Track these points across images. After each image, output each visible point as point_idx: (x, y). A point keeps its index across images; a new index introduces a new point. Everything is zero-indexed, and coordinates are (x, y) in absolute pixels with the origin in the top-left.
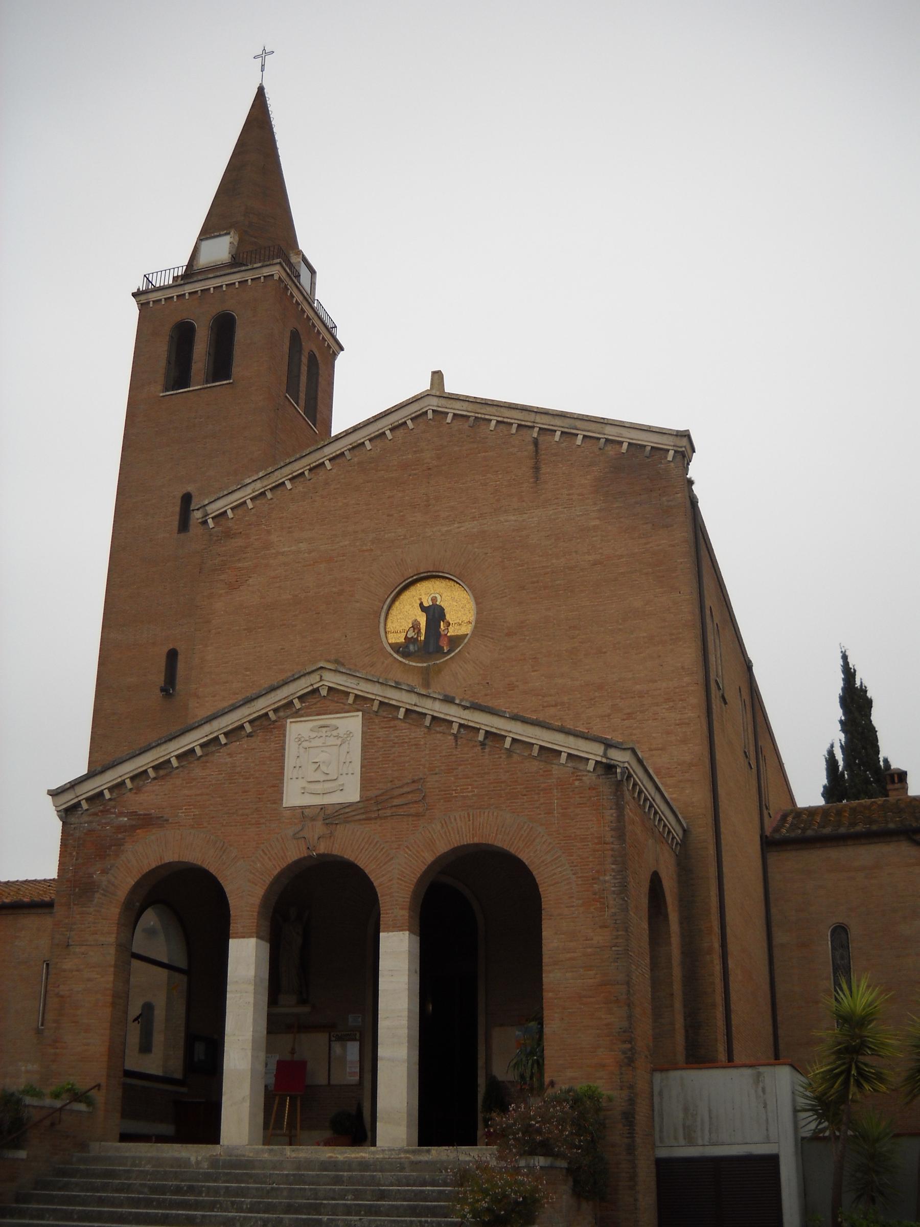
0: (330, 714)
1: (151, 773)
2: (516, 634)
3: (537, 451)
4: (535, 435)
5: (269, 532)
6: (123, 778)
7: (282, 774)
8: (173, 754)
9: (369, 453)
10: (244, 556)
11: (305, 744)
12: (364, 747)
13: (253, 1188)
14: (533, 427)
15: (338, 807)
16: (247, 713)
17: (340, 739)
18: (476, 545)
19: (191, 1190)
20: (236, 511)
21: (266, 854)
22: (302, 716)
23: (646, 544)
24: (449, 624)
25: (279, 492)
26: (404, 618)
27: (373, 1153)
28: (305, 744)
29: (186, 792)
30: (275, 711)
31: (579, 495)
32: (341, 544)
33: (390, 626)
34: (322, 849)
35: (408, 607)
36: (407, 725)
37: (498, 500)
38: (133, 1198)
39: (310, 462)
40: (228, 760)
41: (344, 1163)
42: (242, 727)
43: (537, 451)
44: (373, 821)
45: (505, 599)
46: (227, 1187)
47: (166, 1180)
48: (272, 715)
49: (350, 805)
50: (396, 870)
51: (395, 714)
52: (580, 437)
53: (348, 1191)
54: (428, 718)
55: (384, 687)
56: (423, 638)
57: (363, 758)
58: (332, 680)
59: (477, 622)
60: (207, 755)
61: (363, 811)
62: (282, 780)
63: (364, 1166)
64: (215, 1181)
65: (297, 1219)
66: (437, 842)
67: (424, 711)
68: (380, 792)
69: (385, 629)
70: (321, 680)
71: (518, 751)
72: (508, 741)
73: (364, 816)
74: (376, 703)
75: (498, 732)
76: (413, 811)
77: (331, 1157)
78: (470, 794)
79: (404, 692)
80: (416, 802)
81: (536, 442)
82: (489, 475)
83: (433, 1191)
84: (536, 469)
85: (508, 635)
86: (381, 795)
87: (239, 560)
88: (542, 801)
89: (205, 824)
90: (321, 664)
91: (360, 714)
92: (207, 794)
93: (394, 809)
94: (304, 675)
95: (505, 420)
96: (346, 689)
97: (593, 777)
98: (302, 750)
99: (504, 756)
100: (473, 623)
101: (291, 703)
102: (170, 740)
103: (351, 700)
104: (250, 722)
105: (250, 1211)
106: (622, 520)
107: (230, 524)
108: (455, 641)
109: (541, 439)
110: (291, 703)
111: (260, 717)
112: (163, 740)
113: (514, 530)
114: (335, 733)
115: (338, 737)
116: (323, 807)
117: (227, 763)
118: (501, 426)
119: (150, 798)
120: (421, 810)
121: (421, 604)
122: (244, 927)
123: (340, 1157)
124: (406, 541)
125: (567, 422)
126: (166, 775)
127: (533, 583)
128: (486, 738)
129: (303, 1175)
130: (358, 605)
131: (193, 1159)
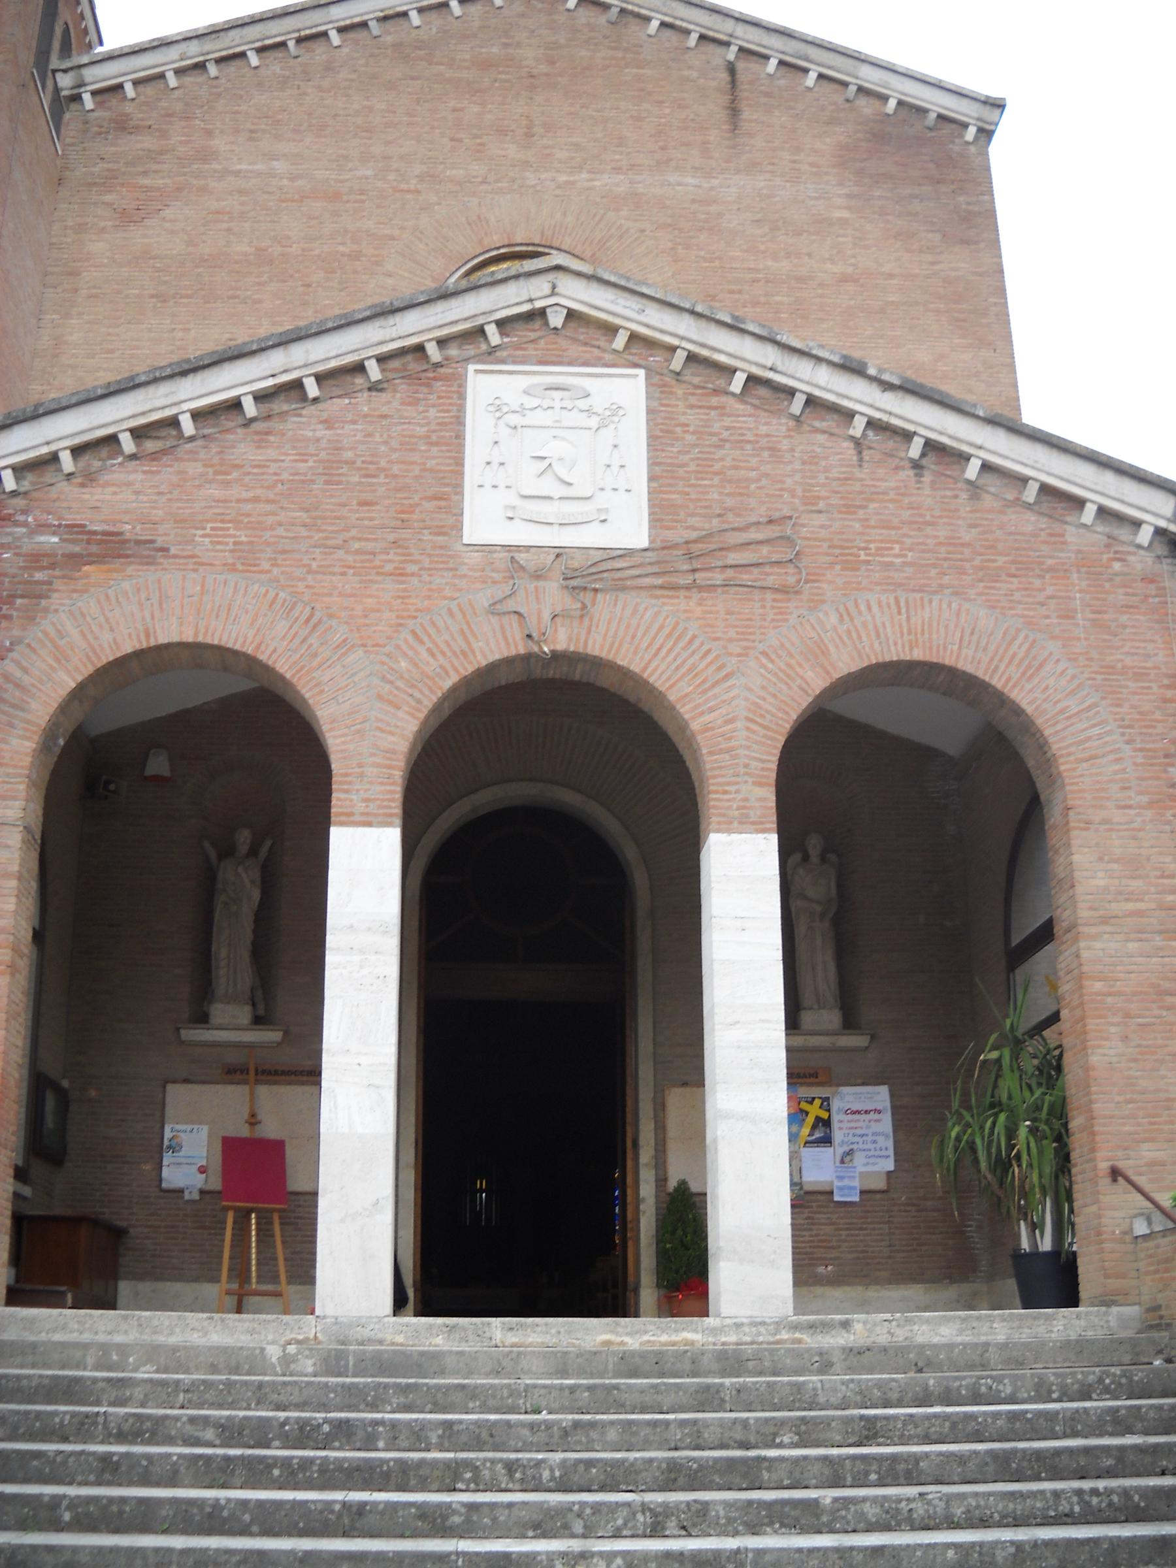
0: (570, 364)
1: (128, 444)
3: (733, 82)
4: (731, 56)
5: (209, 133)
6: (53, 448)
7: (460, 474)
8: (185, 407)
9: (416, 32)
10: (155, 167)
11: (514, 419)
12: (654, 441)
13: (522, 1424)
14: (727, 44)
15: (598, 556)
16: (376, 339)
18: (624, 213)
19: (343, 1432)
20: (141, 88)
21: (422, 642)
22: (503, 361)
23: (933, 263)
25: (232, 68)
27: (714, 1331)
28: (514, 419)
29: (215, 492)
30: (442, 342)
31: (811, 165)
34: (562, 640)
36: (749, 409)
37: (663, 148)
38: (208, 1459)
39: (300, 25)
40: (322, 432)
41: (643, 1355)
42: (359, 368)
43: (733, 82)
44: (682, 593)
46: (449, 1425)
47: (232, 1406)
48: (432, 349)
49: (628, 553)
50: (734, 711)
52: (813, 75)
53: (782, 1422)
54: (800, 400)
55: (703, 324)
57: (653, 463)
58: (577, 294)
60: (269, 417)
61: (656, 569)
62: (458, 488)
63: (692, 1362)
64: (373, 1407)
65: (750, 1503)
66: (832, 650)
68: (694, 535)
70: (553, 293)
71: (992, 490)
73: (659, 581)
74: (680, 356)
75: (955, 444)
76: (771, 581)
77: (608, 1343)
78: (898, 560)
80: (778, 563)
81: (731, 69)
82: (645, 106)
83: (996, 1415)
84: (734, 111)
86: (695, 541)
87: (145, 173)
88: (1050, 590)
89: (266, 565)
91: (641, 373)
92: (268, 501)
93: (730, 573)
95: (678, 23)
96: (610, 319)
97: (1148, 557)
98: (504, 432)
99: (964, 495)
102: (184, 373)
103: (620, 341)
104: (381, 359)
105: (564, 1487)
106: (890, 218)
107: (129, 108)
109: (741, 66)
111: (402, 352)
112: (168, 371)
113: (693, 201)
114: (583, 404)
115: (589, 411)
116: (560, 553)
117: (318, 440)
118: (668, 33)
119: (122, 496)
120: (791, 580)
122: (367, 800)
123: (633, 1343)
125: (792, 46)
126: (164, 452)
127: (731, 292)
129: (616, 1387)
131: (274, 1353)
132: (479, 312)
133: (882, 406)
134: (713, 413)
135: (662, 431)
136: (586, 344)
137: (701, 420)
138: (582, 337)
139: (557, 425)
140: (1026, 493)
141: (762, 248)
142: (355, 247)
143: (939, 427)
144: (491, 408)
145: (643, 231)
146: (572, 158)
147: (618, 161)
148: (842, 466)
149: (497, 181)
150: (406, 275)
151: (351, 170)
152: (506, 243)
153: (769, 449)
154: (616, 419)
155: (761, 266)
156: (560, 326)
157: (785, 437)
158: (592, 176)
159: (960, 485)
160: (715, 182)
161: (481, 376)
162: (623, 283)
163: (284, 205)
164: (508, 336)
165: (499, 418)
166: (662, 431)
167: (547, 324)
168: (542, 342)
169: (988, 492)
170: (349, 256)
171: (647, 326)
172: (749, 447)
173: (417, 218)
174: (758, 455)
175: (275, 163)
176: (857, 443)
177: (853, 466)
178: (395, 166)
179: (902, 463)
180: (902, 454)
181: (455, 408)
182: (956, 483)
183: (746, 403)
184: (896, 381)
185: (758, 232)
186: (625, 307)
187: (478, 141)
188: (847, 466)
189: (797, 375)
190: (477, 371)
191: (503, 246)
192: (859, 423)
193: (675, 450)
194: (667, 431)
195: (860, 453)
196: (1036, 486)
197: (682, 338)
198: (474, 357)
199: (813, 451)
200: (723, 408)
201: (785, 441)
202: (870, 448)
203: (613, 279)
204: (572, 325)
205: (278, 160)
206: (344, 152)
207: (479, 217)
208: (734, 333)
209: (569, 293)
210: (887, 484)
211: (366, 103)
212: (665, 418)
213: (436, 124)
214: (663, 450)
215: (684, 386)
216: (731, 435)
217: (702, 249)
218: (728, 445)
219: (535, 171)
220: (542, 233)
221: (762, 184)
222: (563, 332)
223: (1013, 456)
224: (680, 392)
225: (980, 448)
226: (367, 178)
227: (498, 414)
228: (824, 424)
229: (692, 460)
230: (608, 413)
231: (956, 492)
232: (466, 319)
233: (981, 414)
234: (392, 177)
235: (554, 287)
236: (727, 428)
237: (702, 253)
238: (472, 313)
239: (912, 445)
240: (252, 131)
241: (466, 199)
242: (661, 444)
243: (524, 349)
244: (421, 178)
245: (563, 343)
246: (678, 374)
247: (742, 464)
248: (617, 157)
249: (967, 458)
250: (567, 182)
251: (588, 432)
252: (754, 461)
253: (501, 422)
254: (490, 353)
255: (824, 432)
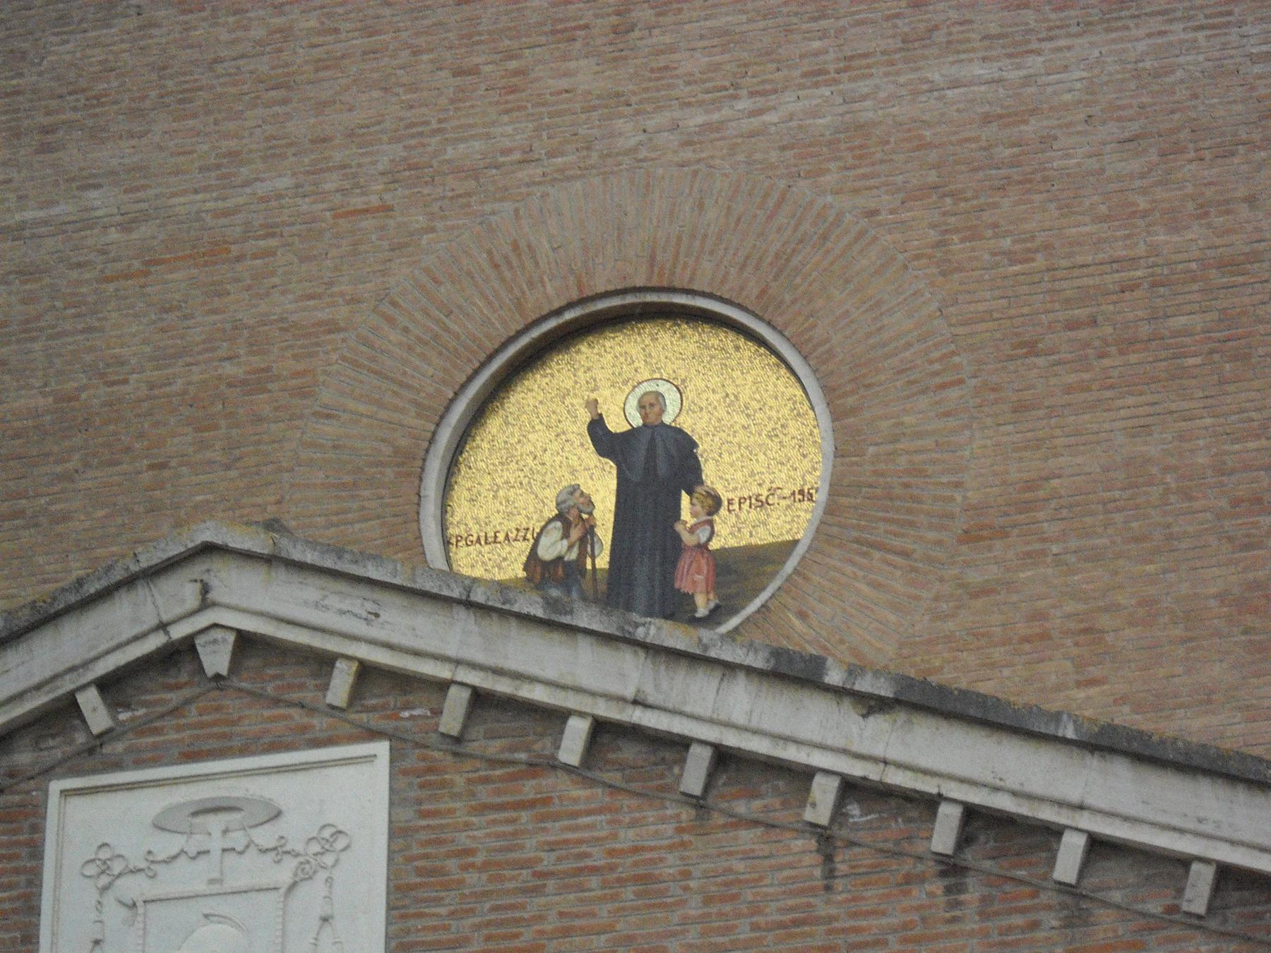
0: (244, 751)
2: (1003, 533)
11: (133, 887)
12: (403, 897)
17: (290, 864)
18: (830, 179)
22: (117, 766)
24: (714, 503)
26: (531, 474)
28: (133, 887)
32: (261, 189)
33: (463, 513)
35: (539, 437)
45: (954, 393)
51: (543, 746)
54: (699, 759)
55: (494, 626)
56: (603, 561)
58: (254, 600)
59: (836, 488)
67: (678, 726)
69: (444, 527)
71: (1116, 896)
72: (1070, 852)
74: (457, 700)
79: (584, 643)
85: (969, 537)
90: (207, 533)
91: (381, 749)
94: (130, 582)
96: (317, 642)
98: (114, 914)
99: (1051, 920)
100: (821, 497)
101: (67, 709)
103: (340, 685)
108: (740, 571)
110: (67, 709)
113: (987, 120)
114: (265, 836)
115: (279, 851)
121: (597, 428)
124: (535, 171)
127: (1072, 325)
128: (965, 840)
130: (329, 429)
132: (61, 668)
133: (864, 749)
134: (525, 816)
135: (420, 872)
136: (276, 702)
137: (499, 836)
138: (270, 689)
139: (215, 888)
140: (1188, 893)
141: (1143, 203)
142: (258, 362)
143: (989, 778)
144: (92, 870)
145: (872, 213)
146: (716, 67)
147: (816, 54)
148: (792, 894)
149: (551, 154)
150: (362, 408)
151: (246, 184)
152: (575, 295)
153: (638, 879)
154: (329, 859)
155: (1141, 249)
156: (224, 672)
157: (671, 848)
158: (760, 102)
159: (1044, 898)
160: (1035, 63)
161: (75, 802)
162: (328, 563)
163: (111, 287)
164: (127, 706)
165: (105, 889)
166: (420, 872)
167: (201, 669)
168: (192, 715)
169: (1106, 904)
170: (244, 383)
171: (390, 646)
172: (594, 881)
173: (384, 273)
174: (614, 898)
175: (94, 194)
176: (824, 837)
177: (811, 891)
178: (338, 157)
179: (920, 867)
180: (920, 847)
181: (23, 878)
182: (1034, 895)
183: (593, 783)
184: (884, 689)
185: (1136, 165)
186: (342, 612)
187: (514, 64)
188: (802, 892)
189: (688, 709)
190: (65, 793)
191: (570, 306)
192: (824, 793)
193: (443, 911)
194: (432, 872)
195: (829, 858)
196: (1208, 873)
197: (458, 662)
198: (60, 763)
199: (729, 870)
200: (547, 801)
201: (671, 858)
202: (852, 844)
203: (310, 557)
204: (253, 663)
205: (97, 186)
206: (233, 144)
207: (516, 247)
208: (556, 636)
209: (233, 600)
210: (884, 921)
211: (278, 21)
212: (429, 843)
213: (422, 41)
214: (421, 915)
215: (468, 765)
216: (559, 859)
217: (1007, 233)
218: (551, 884)
219: (638, 113)
220: (652, 258)
221: (1141, 46)
222: (235, 682)
223: (1151, 816)
224: (459, 780)
225: (1081, 807)
226: (279, 197)
227: (104, 880)
228: (757, 804)
229: (477, 927)
230: (315, 848)
231: (1032, 917)
232: (38, 687)
233: (1070, 733)
234: (331, 183)
235: (205, 589)
236: (551, 847)
237: (1007, 243)
238: (48, 674)
239: (937, 826)
240: (46, 130)
241: (488, 208)
242: (418, 901)
243: (157, 731)
244: (392, 177)
245: (232, 704)
246: (458, 740)
247: (577, 922)
248: (817, 44)
249: (1054, 832)
250: (707, 127)
251: (272, 896)
252: (604, 910)
253: (109, 899)
254: (91, 751)
255: (756, 823)
